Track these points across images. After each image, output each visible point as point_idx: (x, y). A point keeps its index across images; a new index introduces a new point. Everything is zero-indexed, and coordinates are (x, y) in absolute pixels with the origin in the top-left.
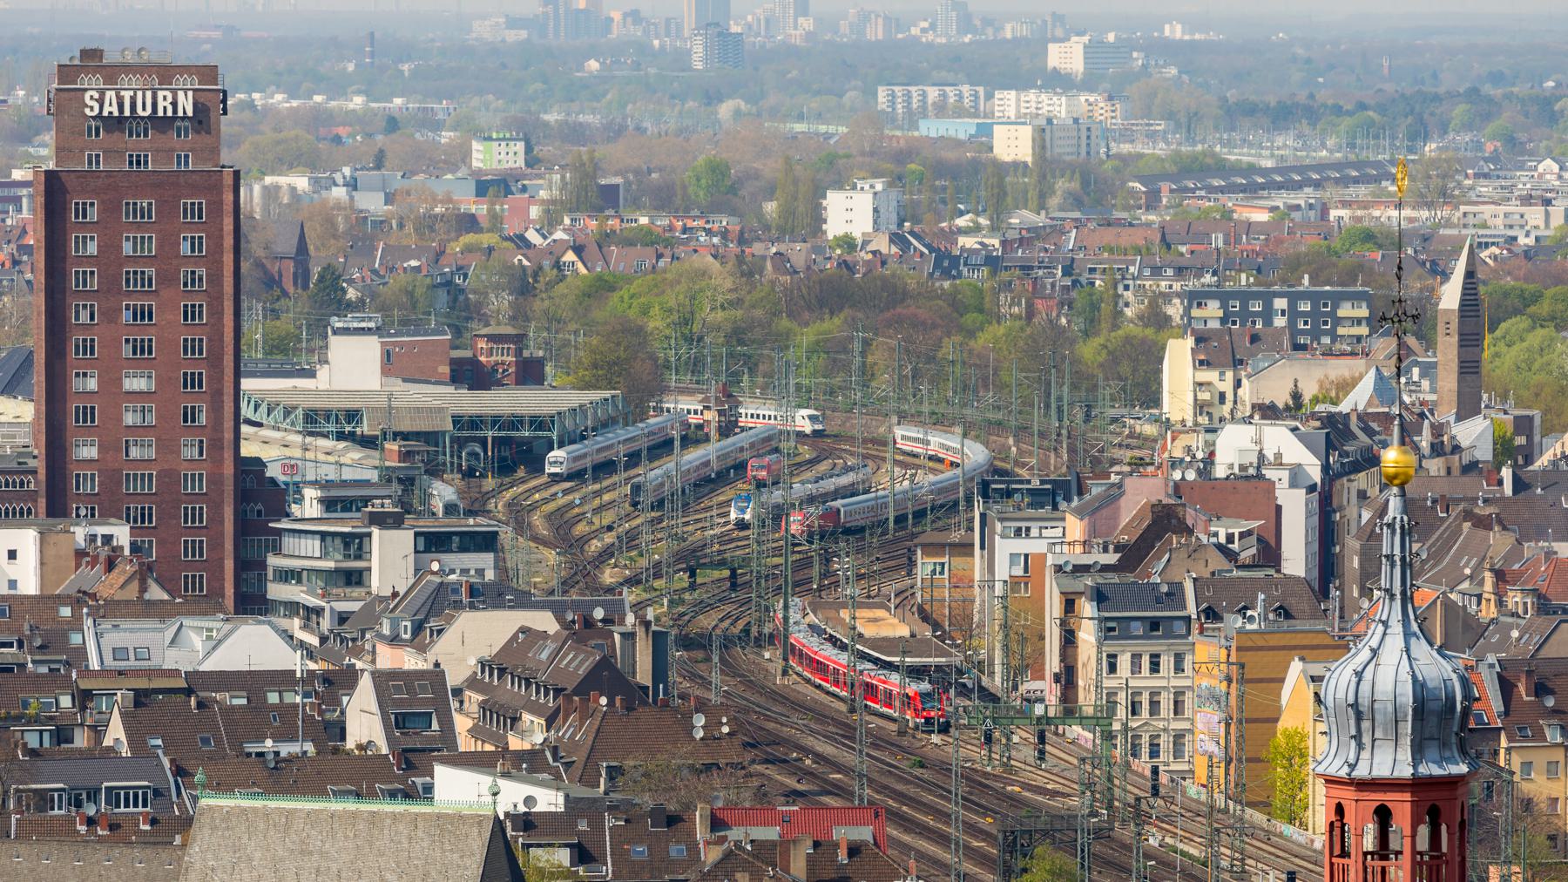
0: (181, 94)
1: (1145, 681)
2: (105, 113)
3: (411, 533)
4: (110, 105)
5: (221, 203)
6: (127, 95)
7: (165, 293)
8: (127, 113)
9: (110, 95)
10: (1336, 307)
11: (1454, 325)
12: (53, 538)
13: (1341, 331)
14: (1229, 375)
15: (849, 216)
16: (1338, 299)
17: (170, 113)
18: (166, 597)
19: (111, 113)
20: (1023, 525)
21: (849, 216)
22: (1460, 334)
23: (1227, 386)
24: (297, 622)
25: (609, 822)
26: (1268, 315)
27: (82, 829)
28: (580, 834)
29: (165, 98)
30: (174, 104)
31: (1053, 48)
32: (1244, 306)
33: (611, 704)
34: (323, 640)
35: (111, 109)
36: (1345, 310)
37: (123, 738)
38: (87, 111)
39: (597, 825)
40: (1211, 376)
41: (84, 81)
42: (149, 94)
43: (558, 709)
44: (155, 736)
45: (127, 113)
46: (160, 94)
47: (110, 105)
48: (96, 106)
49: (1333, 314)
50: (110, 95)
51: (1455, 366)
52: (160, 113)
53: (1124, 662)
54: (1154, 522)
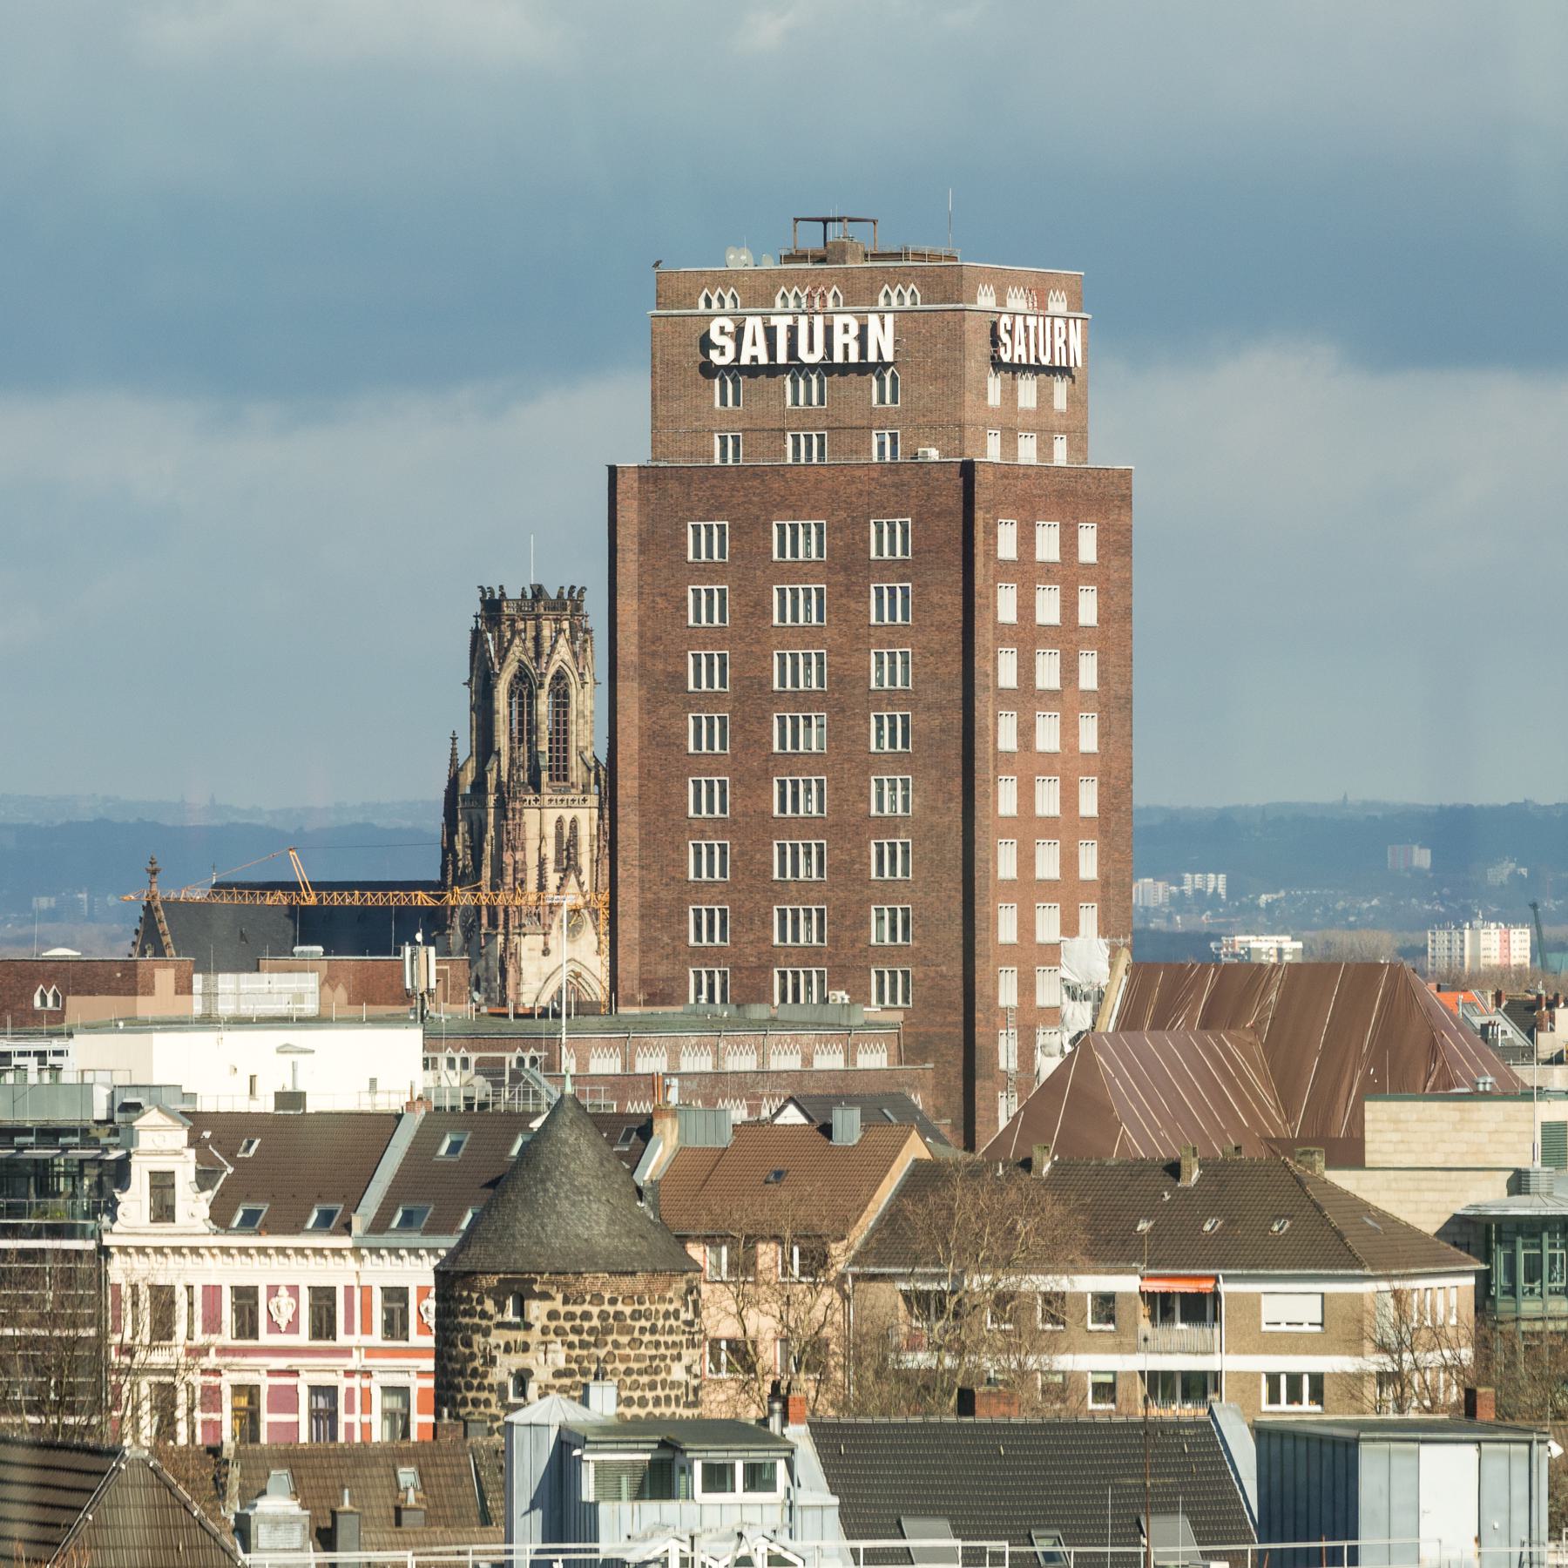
0: (873, 320)
4: (754, 344)
6: (781, 324)
8: (782, 358)
9: (754, 325)
17: (854, 358)
19: (754, 358)
29: (846, 330)
30: (862, 338)
35: (754, 351)
38: (714, 355)
45: (782, 358)
47: (754, 344)
50: (754, 325)
52: (838, 358)
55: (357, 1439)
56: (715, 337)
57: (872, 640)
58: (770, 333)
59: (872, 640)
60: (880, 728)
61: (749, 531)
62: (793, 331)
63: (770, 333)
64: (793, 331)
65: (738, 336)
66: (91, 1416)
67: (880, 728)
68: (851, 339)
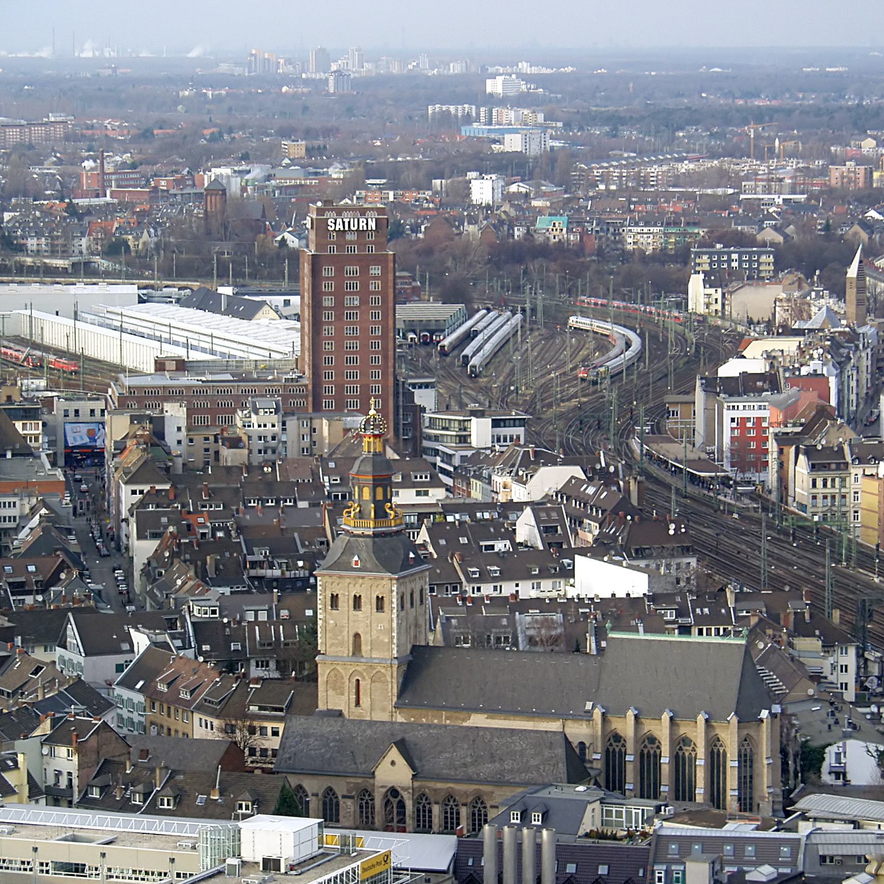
0: (370, 220)
1: (829, 490)
2: (337, 229)
3: (490, 420)
5: (387, 267)
6: (346, 221)
7: (363, 307)
8: (347, 228)
9: (339, 221)
10: (759, 258)
11: (854, 285)
12: (333, 423)
13: (761, 268)
14: (719, 290)
15: (481, 191)
16: (760, 254)
17: (365, 228)
18: (397, 457)
20: (736, 404)
21: (481, 191)
22: (857, 288)
23: (719, 296)
24: (438, 459)
25: (690, 598)
26: (730, 261)
27: (460, 603)
28: (678, 604)
30: (367, 224)
31: (489, 82)
32: (719, 258)
33: (632, 519)
34: (455, 468)
36: (763, 258)
37: (428, 540)
38: (329, 228)
39: (684, 598)
40: (712, 291)
41: (327, 215)
42: (356, 220)
43: (605, 518)
44: (442, 538)
45: (347, 228)
46: (361, 220)
48: (333, 225)
49: (757, 261)
50: (339, 221)
51: (855, 302)
52: (361, 228)
53: (820, 483)
54: (817, 413)
55: (426, 444)
56: (329, 223)
57: (813, 236)
58: (344, 223)
59: (813, 236)
60: (747, 781)
61: (340, 270)
62: (349, 222)
63: (344, 223)
64: (349, 222)
65: (335, 224)
66: (645, 135)
67: (747, 781)
68: (364, 224)
